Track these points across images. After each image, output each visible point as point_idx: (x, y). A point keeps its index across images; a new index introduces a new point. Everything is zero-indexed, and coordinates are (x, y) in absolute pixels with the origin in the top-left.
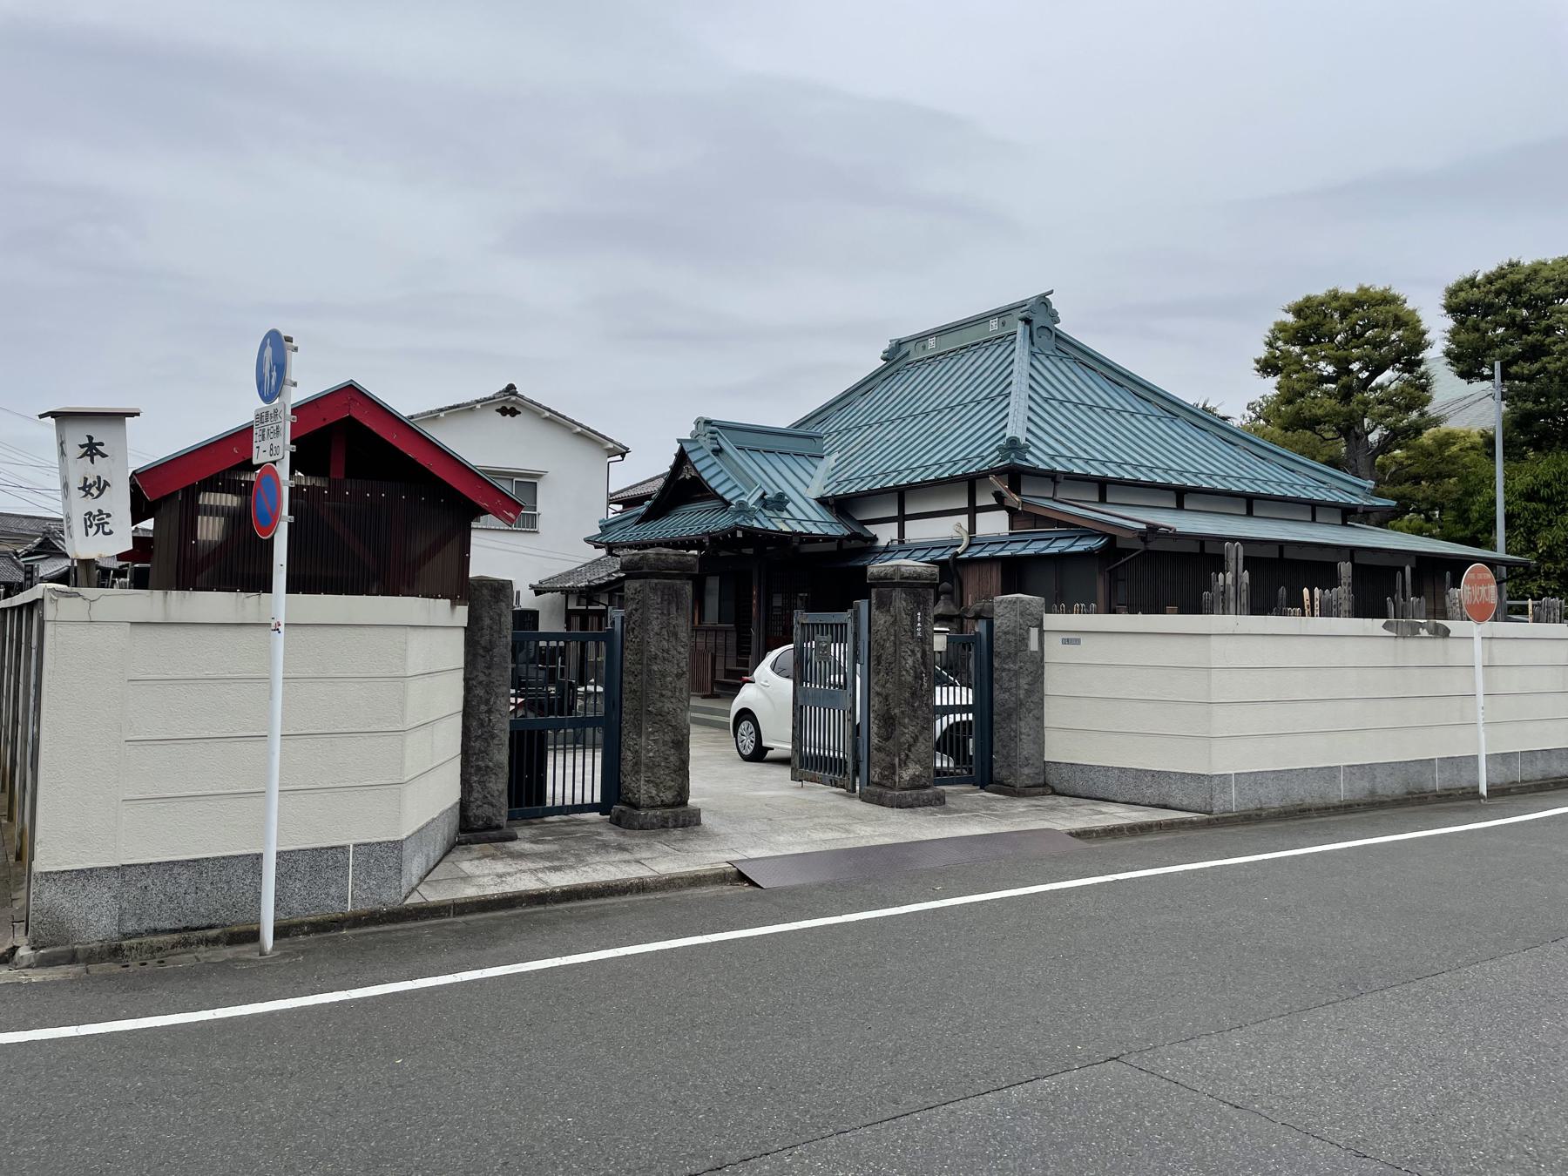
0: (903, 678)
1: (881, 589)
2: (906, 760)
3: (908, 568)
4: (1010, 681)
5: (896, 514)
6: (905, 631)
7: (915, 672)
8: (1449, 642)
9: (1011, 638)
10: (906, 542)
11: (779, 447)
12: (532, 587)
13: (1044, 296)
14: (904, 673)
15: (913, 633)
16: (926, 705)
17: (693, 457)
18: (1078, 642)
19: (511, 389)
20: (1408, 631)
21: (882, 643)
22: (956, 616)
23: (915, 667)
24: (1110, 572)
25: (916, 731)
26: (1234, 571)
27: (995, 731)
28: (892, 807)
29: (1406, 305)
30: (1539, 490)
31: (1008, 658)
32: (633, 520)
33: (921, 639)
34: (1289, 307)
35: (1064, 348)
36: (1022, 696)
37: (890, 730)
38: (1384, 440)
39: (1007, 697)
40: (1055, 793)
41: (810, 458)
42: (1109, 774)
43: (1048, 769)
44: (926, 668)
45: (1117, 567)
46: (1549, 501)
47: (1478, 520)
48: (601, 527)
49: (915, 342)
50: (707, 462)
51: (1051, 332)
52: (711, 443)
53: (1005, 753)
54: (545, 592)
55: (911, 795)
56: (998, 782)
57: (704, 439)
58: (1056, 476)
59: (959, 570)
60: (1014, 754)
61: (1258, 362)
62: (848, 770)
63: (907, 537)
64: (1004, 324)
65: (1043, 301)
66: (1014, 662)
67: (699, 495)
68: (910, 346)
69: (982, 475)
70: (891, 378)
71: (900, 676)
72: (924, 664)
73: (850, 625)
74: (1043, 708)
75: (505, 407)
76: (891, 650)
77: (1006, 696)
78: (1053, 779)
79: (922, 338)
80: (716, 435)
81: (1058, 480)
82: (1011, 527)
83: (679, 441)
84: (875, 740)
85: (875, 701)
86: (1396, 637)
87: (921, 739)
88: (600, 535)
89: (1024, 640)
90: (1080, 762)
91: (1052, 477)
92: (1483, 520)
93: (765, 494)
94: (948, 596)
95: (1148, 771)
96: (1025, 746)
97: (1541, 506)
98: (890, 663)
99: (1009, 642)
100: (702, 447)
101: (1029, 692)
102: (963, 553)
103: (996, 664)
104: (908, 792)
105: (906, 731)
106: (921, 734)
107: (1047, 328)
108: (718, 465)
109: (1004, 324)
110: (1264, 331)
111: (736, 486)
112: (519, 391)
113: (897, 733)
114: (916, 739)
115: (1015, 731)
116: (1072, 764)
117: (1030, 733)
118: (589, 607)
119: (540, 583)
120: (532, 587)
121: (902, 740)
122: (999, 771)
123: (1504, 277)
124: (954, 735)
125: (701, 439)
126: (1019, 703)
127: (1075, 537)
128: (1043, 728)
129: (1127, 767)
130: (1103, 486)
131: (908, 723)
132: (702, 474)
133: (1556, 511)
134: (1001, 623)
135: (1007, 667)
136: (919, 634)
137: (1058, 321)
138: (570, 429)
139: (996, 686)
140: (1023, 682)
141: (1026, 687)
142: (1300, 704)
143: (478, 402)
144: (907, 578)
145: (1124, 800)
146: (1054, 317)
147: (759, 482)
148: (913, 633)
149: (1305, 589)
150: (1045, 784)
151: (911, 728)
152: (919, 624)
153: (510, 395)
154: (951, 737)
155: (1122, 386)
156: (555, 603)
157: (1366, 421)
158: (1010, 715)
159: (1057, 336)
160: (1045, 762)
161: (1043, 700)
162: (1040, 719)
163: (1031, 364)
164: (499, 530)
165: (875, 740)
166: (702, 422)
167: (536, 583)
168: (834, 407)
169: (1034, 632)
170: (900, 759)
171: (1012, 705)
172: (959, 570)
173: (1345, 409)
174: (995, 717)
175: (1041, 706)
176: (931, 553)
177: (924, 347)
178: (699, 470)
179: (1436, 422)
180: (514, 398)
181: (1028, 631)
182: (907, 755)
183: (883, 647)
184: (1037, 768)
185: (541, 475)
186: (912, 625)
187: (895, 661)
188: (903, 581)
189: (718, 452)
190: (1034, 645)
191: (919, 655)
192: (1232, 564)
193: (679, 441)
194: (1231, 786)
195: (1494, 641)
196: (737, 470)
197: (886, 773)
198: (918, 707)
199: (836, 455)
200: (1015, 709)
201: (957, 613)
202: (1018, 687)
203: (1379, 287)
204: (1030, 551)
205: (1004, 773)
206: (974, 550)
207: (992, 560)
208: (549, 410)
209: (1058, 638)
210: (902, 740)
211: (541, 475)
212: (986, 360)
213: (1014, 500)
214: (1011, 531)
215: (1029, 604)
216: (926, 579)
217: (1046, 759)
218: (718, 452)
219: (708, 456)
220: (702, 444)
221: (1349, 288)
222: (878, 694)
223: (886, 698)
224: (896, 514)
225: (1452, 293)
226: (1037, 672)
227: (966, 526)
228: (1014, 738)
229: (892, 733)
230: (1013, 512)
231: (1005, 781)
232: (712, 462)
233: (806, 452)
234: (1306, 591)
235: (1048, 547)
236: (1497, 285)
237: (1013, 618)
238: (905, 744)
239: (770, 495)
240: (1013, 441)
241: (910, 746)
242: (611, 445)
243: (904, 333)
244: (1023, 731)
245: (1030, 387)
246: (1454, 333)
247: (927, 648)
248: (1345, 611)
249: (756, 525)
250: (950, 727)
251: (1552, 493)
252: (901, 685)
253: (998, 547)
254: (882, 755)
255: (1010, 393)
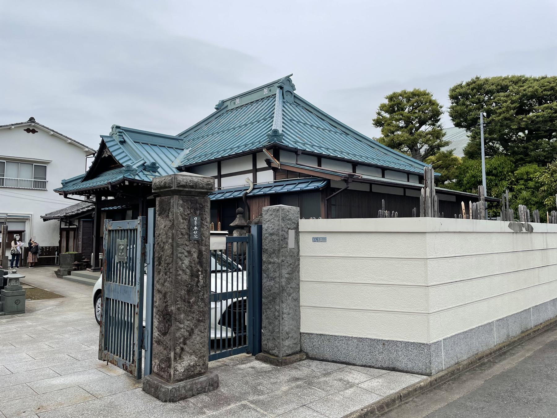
0: (180, 278)
1: (163, 198)
2: (181, 353)
3: (184, 178)
4: (275, 271)
5: (251, 168)
6: (182, 234)
7: (192, 271)
8: (533, 234)
9: (274, 237)
10: (222, 189)
11: (159, 143)
12: (41, 217)
13: (288, 77)
14: (180, 272)
15: (190, 236)
16: (202, 299)
17: (108, 145)
18: (324, 240)
19: (32, 120)
20: (517, 229)
21: (162, 245)
22: (246, 226)
23: (191, 266)
24: (327, 200)
25: (191, 325)
26: (430, 187)
27: (264, 310)
28: (166, 401)
29: (432, 97)
30: (492, 171)
31: (274, 253)
32: (80, 180)
33: (198, 241)
34: (387, 96)
35: (298, 102)
36: (284, 284)
37: (167, 326)
38: (428, 151)
39: (272, 284)
40: (309, 357)
41: (176, 150)
42: (349, 343)
43: (303, 338)
44: (201, 266)
45: (331, 198)
46: (496, 175)
47: (466, 184)
48: (62, 184)
49: (230, 101)
50: (117, 147)
51: (292, 94)
52: (119, 138)
53: (271, 329)
54: (49, 219)
55: (184, 387)
56: (268, 352)
57: (115, 136)
58: (297, 151)
59: (248, 201)
60: (278, 330)
61: (374, 120)
62: (135, 358)
63: (222, 186)
64: (270, 90)
65: (288, 79)
66: (278, 257)
67: (114, 166)
68: (228, 103)
69: (260, 150)
70: (219, 117)
71: (177, 275)
72: (200, 263)
73: (139, 229)
74: (299, 292)
75: (29, 129)
76: (169, 252)
77: (272, 283)
78: (307, 348)
79: (234, 99)
80: (122, 134)
81: (298, 153)
82: (275, 178)
83: (101, 136)
84: (156, 334)
85: (157, 297)
86: (513, 233)
87: (196, 331)
88: (62, 188)
89: (285, 239)
90: (327, 333)
91: (295, 152)
92: (469, 184)
93: (145, 163)
94: (241, 215)
95: (380, 340)
96: (286, 322)
97: (493, 178)
98: (168, 264)
99: (274, 241)
100: (114, 140)
101: (289, 280)
102: (250, 193)
103: (264, 259)
104: (182, 384)
105: (182, 326)
106: (196, 327)
107: (290, 92)
108: (122, 149)
109: (270, 90)
110: (376, 109)
111: (130, 159)
112: (37, 121)
113: (172, 328)
114: (191, 333)
115: (279, 312)
116: (321, 335)
117: (290, 312)
118: (70, 227)
119: (46, 215)
120: (41, 217)
121: (178, 335)
122: (267, 343)
123: (474, 82)
124: (237, 311)
125: (114, 136)
126: (281, 289)
127: (308, 182)
128: (299, 307)
129: (363, 337)
130: (320, 158)
131: (184, 318)
132: (113, 153)
133: (499, 180)
134: (268, 227)
135: (272, 261)
136: (196, 237)
137: (295, 90)
138: (66, 141)
139: (264, 275)
140: (284, 272)
141: (287, 276)
142: (474, 281)
143: (13, 125)
144: (184, 186)
145: (361, 363)
146: (293, 87)
147: (143, 157)
148: (190, 236)
149: (462, 202)
150: (301, 351)
151: (187, 323)
152: (196, 228)
153: (32, 122)
154: (235, 313)
155: (324, 120)
156: (56, 225)
157: (418, 145)
158: (274, 299)
159: (294, 96)
160: (301, 333)
161: (299, 285)
162: (297, 300)
163: (283, 106)
164: (27, 189)
165: (156, 334)
166: (115, 127)
167: (44, 215)
168: (192, 130)
169: (292, 233)
170: (175, 353)
171: (276, 291)
172: (248, 201)
173: (412, 138)
174: (263, 299)
175: (297, 290)
176: (234, 194)
177: (234, 103)
178: (111, 151)
179: (447, 144)
180: (33, 124)
181: (287, 233)
182: (182, 349)
183: (163, 249)
184: (295, 339)
185: (49, 163)
186: (189, 229)
187: (172, 261)
188: (181, 189)
189: (123, 142)
190: (291, 244)
191: (195, 255)
192: (429, 182)
193: (101, 136)
194: (441, 350)
195: (547, 234)
196: (132, 151)
197: (163, 366)
198: (194, 303)
199: (190, 149)
200: (279, 294)
201: (246, 224)
202: (280, 276)
203: (422, 90)
204: (285, 189)
205: (270, 345)
206: (256, 191)
207: (265, 195)
208: (53, 131)
209: (310, 237)
210: (178, 335)
211: (49, 163)
212: (263, 107)
213: (276, 163)
214: (275, 181)
215: (288, 211)
216: (203, 188)
217: (302, 331)
218: (123, 142)
219: (117, 144)
220: (114, 138)
221: (410, 89)
222: (159, 291)
223: (165, 296)
224: (216, 174)
225: (453, 90)
226: (295, 263)
227: (251, 179)
228: (278, 317)
229: (169, 329)
230: (275, 170)
231: (271, 352)
232: (122, 151)
233: (174, 147)
234: (463, 203)
235: (294, 188)
236: (471, 86)
237: (277, 223)
238: (180, 338)
239: (148, 163)
240: (276, 131)
241: (185, 339)
242: (87, 149)
243: (225, 98)
244: (285, 311)
245: (283, 114)
246: (452, 108)
247: (203, 248)
248: (483, 217)
249: (137, 178)
250: (229, 308)
251: (497, 172)
252: (177, 283)
253: (268, 189)
254: (161, 348)
255: (274, 117)
